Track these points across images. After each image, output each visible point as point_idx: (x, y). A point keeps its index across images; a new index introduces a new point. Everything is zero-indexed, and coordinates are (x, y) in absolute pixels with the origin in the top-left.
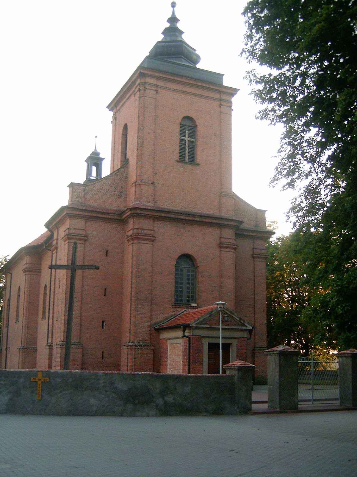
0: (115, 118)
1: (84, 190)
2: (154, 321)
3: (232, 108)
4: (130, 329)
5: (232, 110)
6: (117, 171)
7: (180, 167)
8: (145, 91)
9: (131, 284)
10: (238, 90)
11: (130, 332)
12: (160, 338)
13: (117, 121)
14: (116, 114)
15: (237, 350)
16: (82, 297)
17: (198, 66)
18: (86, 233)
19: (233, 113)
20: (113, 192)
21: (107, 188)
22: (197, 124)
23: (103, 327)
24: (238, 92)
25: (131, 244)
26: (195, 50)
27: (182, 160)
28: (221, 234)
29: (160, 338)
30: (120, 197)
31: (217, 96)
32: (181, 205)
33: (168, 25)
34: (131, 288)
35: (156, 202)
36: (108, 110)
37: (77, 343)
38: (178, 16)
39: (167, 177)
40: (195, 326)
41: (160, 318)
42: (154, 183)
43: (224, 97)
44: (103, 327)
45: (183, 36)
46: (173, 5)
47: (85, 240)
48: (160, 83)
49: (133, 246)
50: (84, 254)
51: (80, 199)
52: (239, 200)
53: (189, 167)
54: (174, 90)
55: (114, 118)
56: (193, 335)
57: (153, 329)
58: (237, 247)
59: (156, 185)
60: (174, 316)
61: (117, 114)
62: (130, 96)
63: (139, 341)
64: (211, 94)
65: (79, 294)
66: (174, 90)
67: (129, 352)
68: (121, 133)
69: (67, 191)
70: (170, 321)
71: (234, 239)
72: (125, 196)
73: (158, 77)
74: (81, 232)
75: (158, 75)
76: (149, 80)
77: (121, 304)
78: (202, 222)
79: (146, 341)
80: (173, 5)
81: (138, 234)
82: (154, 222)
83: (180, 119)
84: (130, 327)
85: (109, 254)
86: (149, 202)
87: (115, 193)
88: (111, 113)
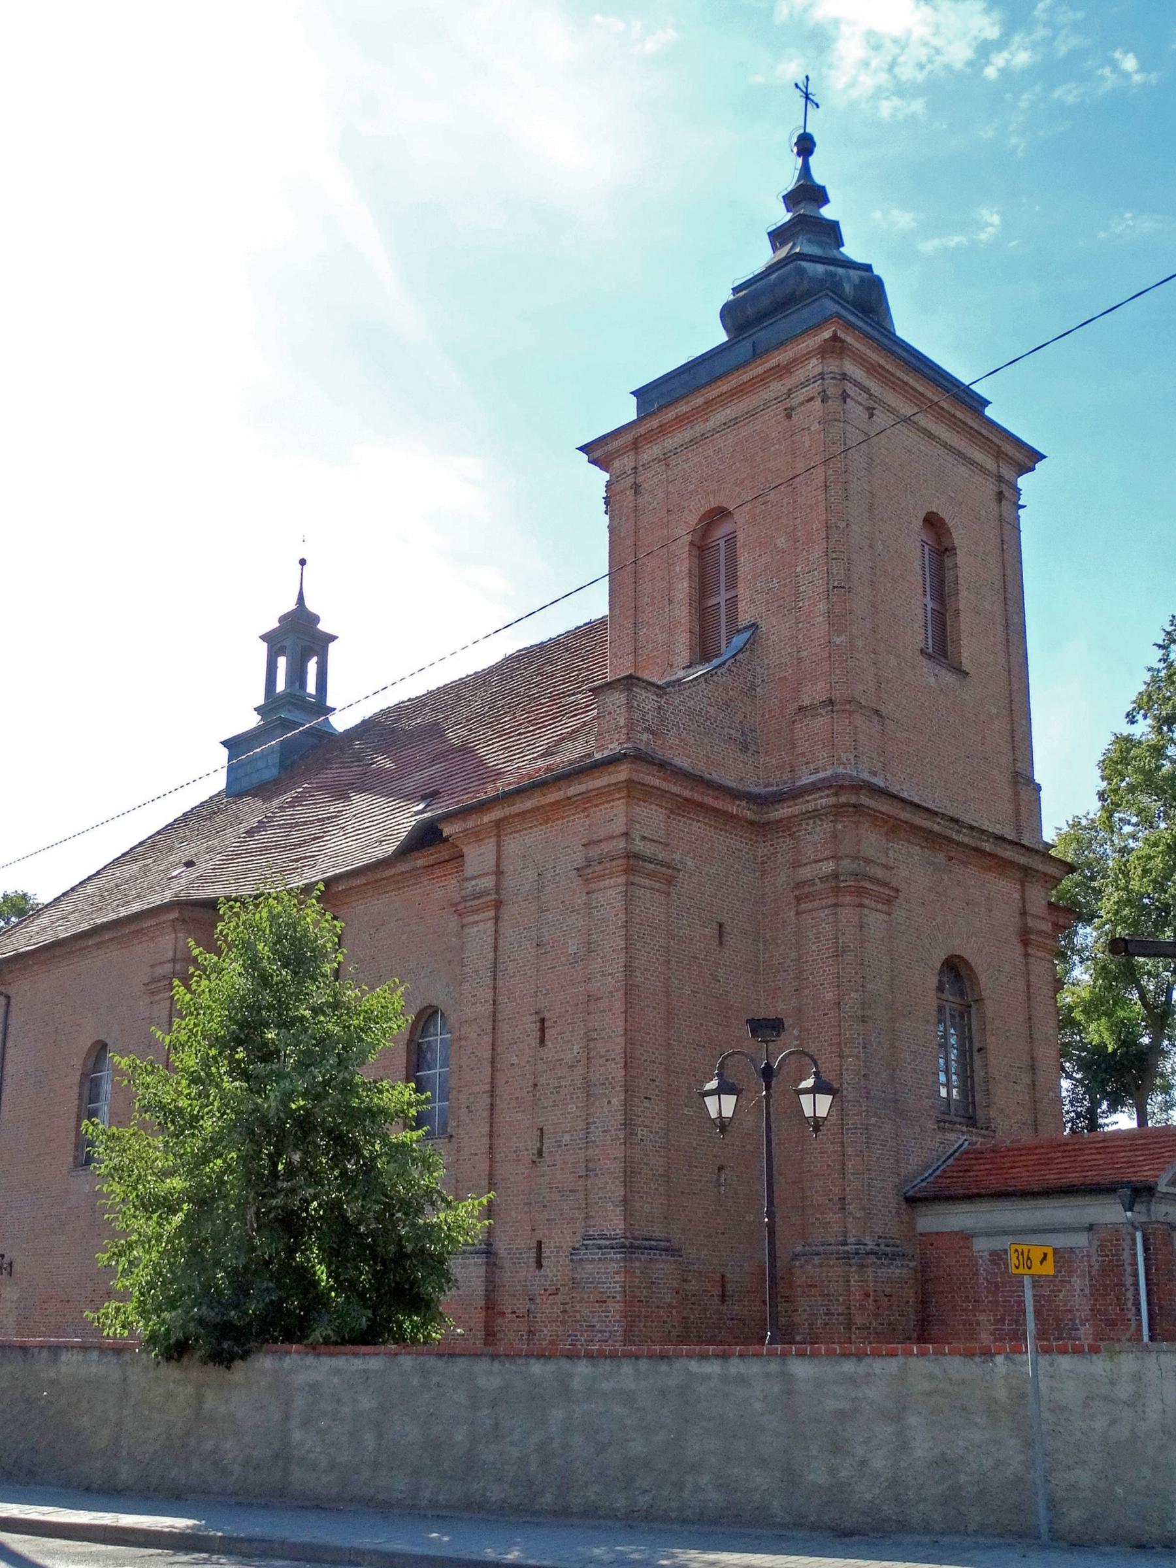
46: (805, 146)
51: (651, 737)
80: (805, 146)
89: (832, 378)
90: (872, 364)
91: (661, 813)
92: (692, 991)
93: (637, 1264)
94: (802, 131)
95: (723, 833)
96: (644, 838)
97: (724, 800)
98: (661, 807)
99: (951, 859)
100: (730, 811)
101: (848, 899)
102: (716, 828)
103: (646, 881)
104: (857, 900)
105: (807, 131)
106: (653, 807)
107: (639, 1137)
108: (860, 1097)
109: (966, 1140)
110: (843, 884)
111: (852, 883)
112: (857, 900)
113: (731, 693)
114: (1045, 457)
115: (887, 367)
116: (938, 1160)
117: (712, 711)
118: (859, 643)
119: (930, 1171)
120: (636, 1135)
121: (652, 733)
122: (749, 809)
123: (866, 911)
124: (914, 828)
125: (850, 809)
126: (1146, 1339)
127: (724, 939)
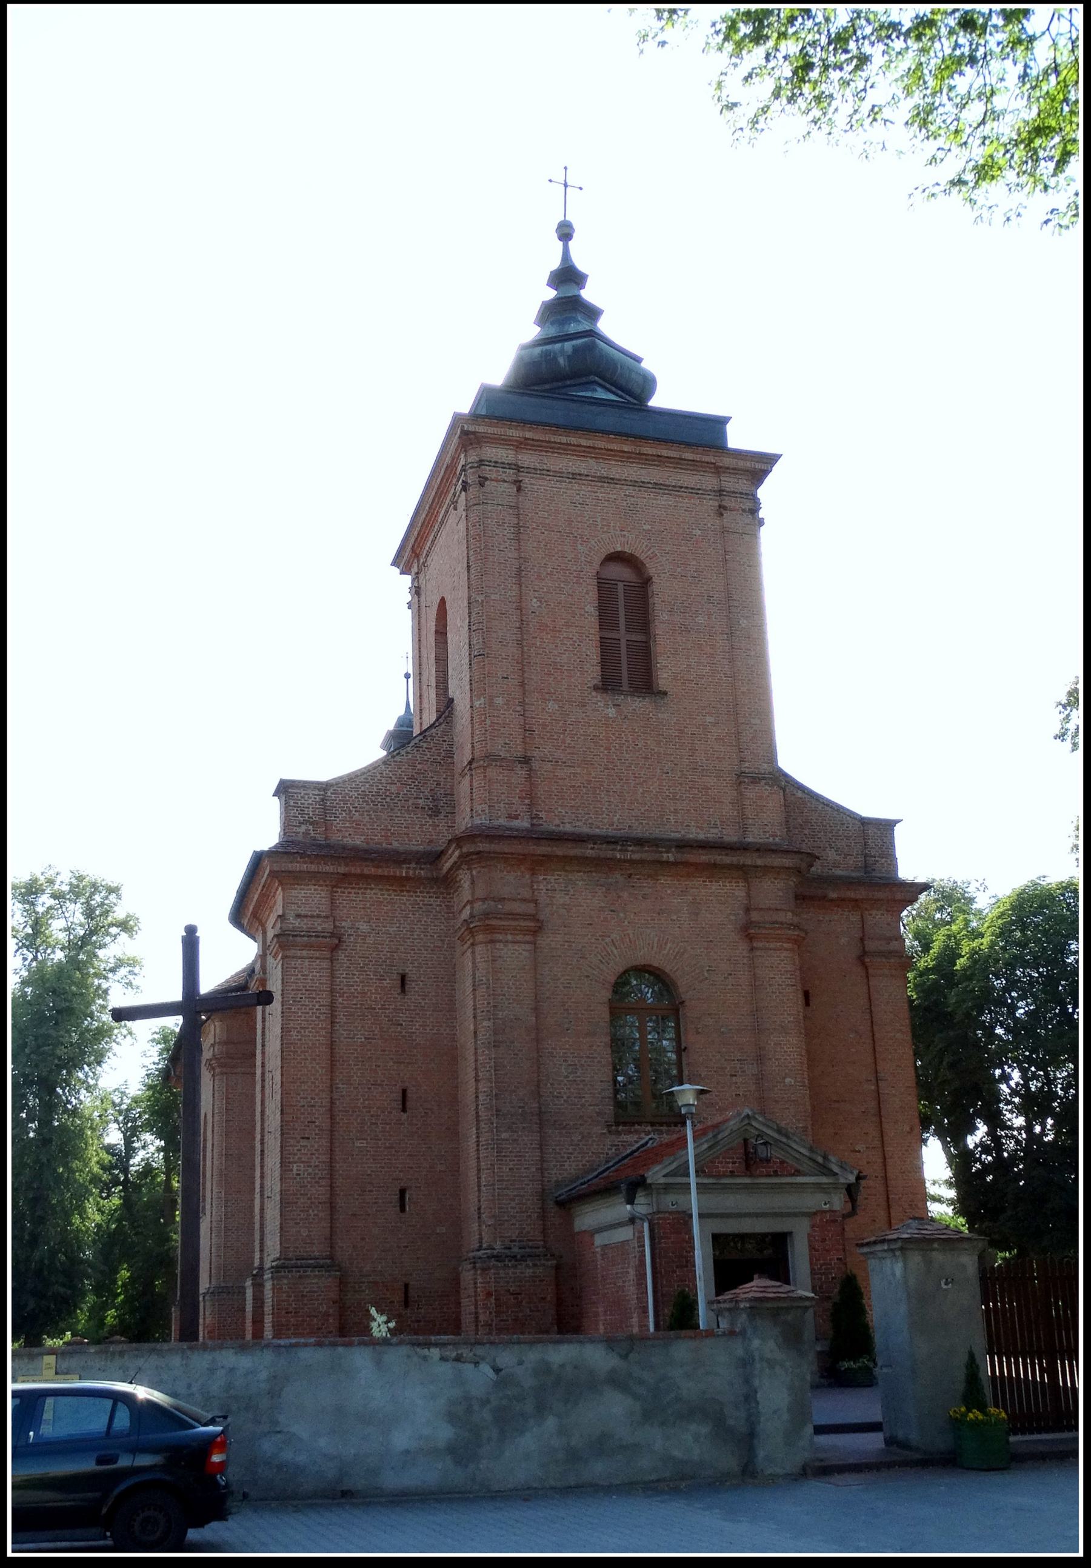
0: (416, 591)
1: (323, 800)
2: (555, 1174)
3: (761, 514)
4: (479, 1209)
5: (761, 522)
6: (421, 737)
7: (605, 707)
8: (482, 485)
9: (476, 1069)
10: (729, 418)
11: (479, 1218)
12: (577, 1230)
13: (423, 598)
14: (417, 577)
15: (810, 1251)
16: (332, 1117)
17: (654, 402)
18: (335, 927)
19: (764, 533)
20: (411, 802)
21: (394, 789)
22: (652, 572)
23: (403, 1209)
24: (776, 468)
25: (469, 948)
26: (639, 360)
27: (608, 684)
28: (749, 896)
29: (577, 1230)
30: (435, 812)
31: (709, 482)
32: (615, 819)
33: (551, 294)
34: (477, 1081)
35: (537, 817)
36: (397, 571)
37: (322, 1262)
38: (580, 263)
39: (568, 740)
40: (662, 1181)
41: (571, 1168)
42: (526, 760)
43: (730, 483)
44: (403, 1209)
45: (643, 365)
46: (565, 232)
47: (335, 948)
48: (527, 459)
49: (473, 953)
50: (332, 991)
51: (311, 827)
52: (804, 796)
53: (638, 704)
54: (575, 476)
55: (414, 590)
56: (659, 1212)
57: (551, 1204)
58: (803, 934)
59: (535, 765)
60: (617, 1159)
61: (421, 576)
62: (447, 512)
63: (507, 1243)
64: (689, 479)
65: (322, 1110)
66: (575, 476)
67: (480, 1280)
68: (433, 629)
69: (274, 806)
70: (605, 1174)
71: (792, 912)
72: (448, 810)
73: (521, 443)
74: (320, 926)
75: (516, 433)
76: (491, 452)
77: (453, 1133)
78: (686, 864)
79: (530, 1243)
80: (565, 232)
81: (486, 915)
82: (533, 873)
83: (597, 560)
84: (479, 1201)
85: (410, 986)
86: (516, 817)
87: (420, 801)
88: (407, 580)
89: (471, 468)
90: (516, 441)
91: (322, 890)
92: (365, 1038)
93: (285, 1281)
94: (563, 219)
95: (405, 893)
96: (298, 916)
97: (388, 867)
98: (321, 886)
99: (630, 876)
100: (398, 874)
101: (480, 937)
102: (395, 891)
103: (304, 952)
104: (489, 937)
105: (567, 219)
106: (313, 887)
107: (295, 1172)
108: (492, 1115)
109: (651, 1139)
110: (472, 926)
111: (478, 924)
112: (489, 937)
113: (419, 767)
114: (779, 456)
115: (536, 438)
116: (607, 1162)
117: (394, 789)
118: (499, 701)
119: (596, 1173)
120: (292, 1170)
121: (311, 823)
122: (421, 869)
123: (498, 945)
124: (567, 860)
125: (474, 857)
126: (249, 1336)
127: (407, 987)
